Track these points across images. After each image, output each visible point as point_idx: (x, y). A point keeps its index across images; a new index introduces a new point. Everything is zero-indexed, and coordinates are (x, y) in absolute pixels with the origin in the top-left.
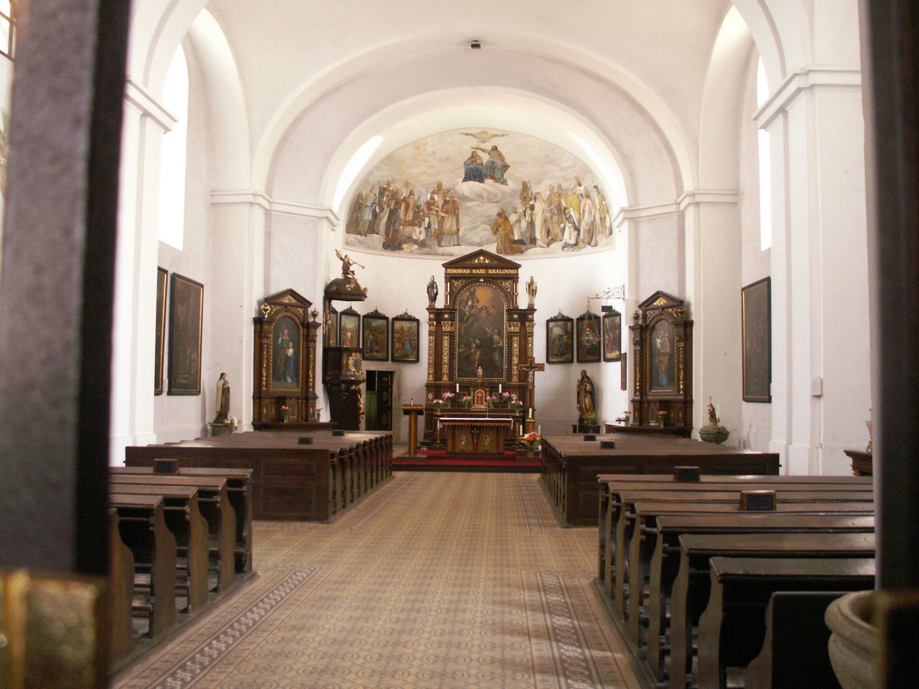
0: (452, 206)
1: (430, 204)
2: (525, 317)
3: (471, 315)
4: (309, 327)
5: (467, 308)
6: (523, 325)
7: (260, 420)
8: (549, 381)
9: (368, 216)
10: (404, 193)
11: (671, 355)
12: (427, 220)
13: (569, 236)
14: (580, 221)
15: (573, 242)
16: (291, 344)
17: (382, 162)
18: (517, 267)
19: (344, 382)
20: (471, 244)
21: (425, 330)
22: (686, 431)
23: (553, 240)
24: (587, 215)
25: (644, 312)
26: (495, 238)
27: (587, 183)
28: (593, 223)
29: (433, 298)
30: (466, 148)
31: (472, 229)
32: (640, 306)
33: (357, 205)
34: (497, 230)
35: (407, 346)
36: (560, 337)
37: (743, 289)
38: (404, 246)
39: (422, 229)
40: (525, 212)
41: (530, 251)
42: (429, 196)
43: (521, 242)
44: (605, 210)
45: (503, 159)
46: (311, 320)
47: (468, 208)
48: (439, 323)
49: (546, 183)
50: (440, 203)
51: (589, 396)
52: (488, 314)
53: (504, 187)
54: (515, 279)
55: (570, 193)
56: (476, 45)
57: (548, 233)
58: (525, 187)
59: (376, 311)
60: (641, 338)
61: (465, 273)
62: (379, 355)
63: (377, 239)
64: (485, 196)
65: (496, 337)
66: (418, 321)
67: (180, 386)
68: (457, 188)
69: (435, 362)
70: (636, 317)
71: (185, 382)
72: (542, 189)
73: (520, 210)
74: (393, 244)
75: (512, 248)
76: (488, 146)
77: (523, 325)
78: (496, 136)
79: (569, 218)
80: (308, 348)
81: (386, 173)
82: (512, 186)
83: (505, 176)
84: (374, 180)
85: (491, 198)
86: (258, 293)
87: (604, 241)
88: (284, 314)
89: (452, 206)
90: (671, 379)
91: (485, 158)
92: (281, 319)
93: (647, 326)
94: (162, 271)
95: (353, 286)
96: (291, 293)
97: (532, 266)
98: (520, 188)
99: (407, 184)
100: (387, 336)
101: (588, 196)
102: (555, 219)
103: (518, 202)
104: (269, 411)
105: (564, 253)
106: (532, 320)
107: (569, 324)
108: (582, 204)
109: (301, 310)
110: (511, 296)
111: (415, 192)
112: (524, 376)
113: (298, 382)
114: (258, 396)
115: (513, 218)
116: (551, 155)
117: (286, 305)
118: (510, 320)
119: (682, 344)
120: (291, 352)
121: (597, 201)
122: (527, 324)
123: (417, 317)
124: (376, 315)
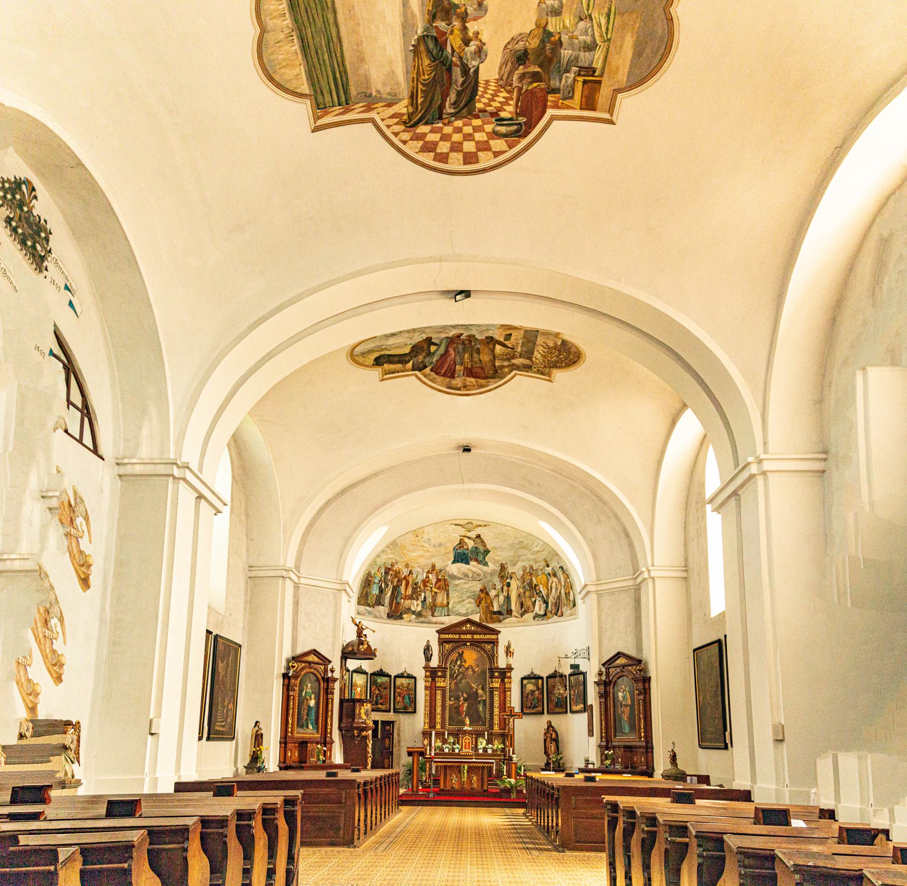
0: (443, 584)
1: (425, 582)
2: (505, 674)
3: (459, 673)
4: (328, 681)
5: (456, 667)
6: (503, 681)
7: (284, 762)
8: (528, 731)
9: (375, 591)
10: (405, 572)
11: (632, 706)
12: (423, 594)
13: (539, 608)
14: (548, 596)
15: (542, 612)
16: (313, 696)
17: (387, 547)
18: (497, 632)
19: (357, 728)
20: (459, 614)
21: (421, 685)
22: (649, 772)
23: (526, 612)
24: (554, 590)
25: (607, 669)
26: (478, 610)
27: (554, 564)
28: (559, 597)
29: (428, 659)
30: (455, 535)
31: (459, 602)
32: (603, 665)
33: (367, 582)
34: (480, 602)
35: (407, 700)
36: (533, 692)
37: (695, 650)
38: (404, 616)
39: (419, 602)
40: (502, 588)
41: (506, 621)
42: (425, 575)
43: (500, 613)
44: (569, 586)
45: (485, 546)
46: (330, 675)
47: (457, 585)
48: (433, 680)
49: (520, 564)
50: (434, 581)
51: (554, 743)
52: (474, 672)
53: (485, 568)
54: (495, 643)
55: (540, 573)
56: (467, 450)
57: (522, 605)
58: (503, 567)
59: (381, 670)
60: (606, 692)
61: (453, 638)
62: (383, 707)
63: (383, 610)
64: (470, 575)
65: (480, 692)
66: (415, 678)
67: (218, 732)
68: (447, 569)
69: (430, 712)
70: (600, 674)
71: (222, 729)
72: (516, 569)
73: (499, 587)
74: (395, 614)
75: (492, 618)
76: (473, 534)
77: (503, 681)
78: (480, 526)
79: (539, 593)
80: (327, 699)
81: (391, 556)
82: (492, 567)
83: (487, 559)
84: (380, 562)
85: (476, 577)
86: (287, 653)
87: (569, 612)
88: (308, 670)
89: (443, 584)
90: (632, 727)
91: (470, 544)
92: (304, 673)
93: (610, 682)
94: (209, 632)
95: (366, 646)
96: (315, 652)
97: (509, 633)
98: (498, 569)
99: (407, 566)
100: (390, 691)
101: (555, 575)
102: (527, 594)
103: (496, 580)
104: (294, 755)
105: (535, 622)
106: (510, 678)
107: (540, 681)
108: (550, 581)
109: (323, 667)
110: (492, 657)
111: (414, 571)
112: (504, 724)
113: (317, 729)
114: (284, 742)
115: (493, 593)
116: (523, 543)
117: (310, 663)
118: (492, 677)
119: (642, 697)
120: (312, 703)
121: (562, 579)
122: (506, 680)
123: (414, 675)
124: (381, 673)
